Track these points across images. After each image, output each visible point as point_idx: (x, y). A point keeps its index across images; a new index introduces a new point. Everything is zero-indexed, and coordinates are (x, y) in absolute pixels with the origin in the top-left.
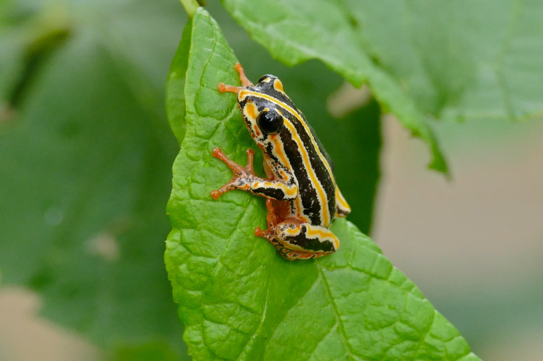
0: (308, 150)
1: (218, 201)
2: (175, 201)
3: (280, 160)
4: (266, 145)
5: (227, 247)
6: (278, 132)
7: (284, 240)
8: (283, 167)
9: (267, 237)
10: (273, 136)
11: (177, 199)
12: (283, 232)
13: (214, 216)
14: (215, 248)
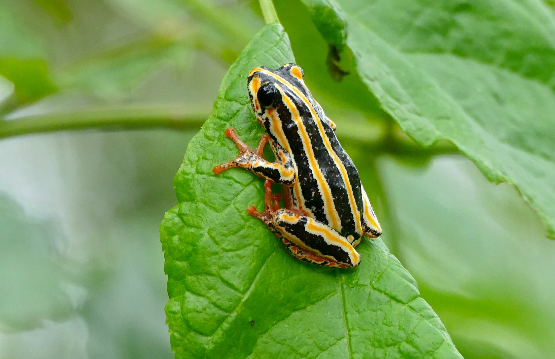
0: (311, 138)
1: (219, 177)
2: (182, 175)
3: (279, 140)
4: (264, 120)
5: (217, 220)
6: (275, 107)
7: (278, 225)
8: (283, 148)
9: (261, 219)
10: (270, 111)
11: (184, 173)
12: (277, 216)
13: (212, 190)
14: (207, 220)
